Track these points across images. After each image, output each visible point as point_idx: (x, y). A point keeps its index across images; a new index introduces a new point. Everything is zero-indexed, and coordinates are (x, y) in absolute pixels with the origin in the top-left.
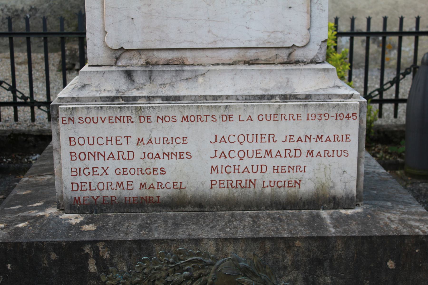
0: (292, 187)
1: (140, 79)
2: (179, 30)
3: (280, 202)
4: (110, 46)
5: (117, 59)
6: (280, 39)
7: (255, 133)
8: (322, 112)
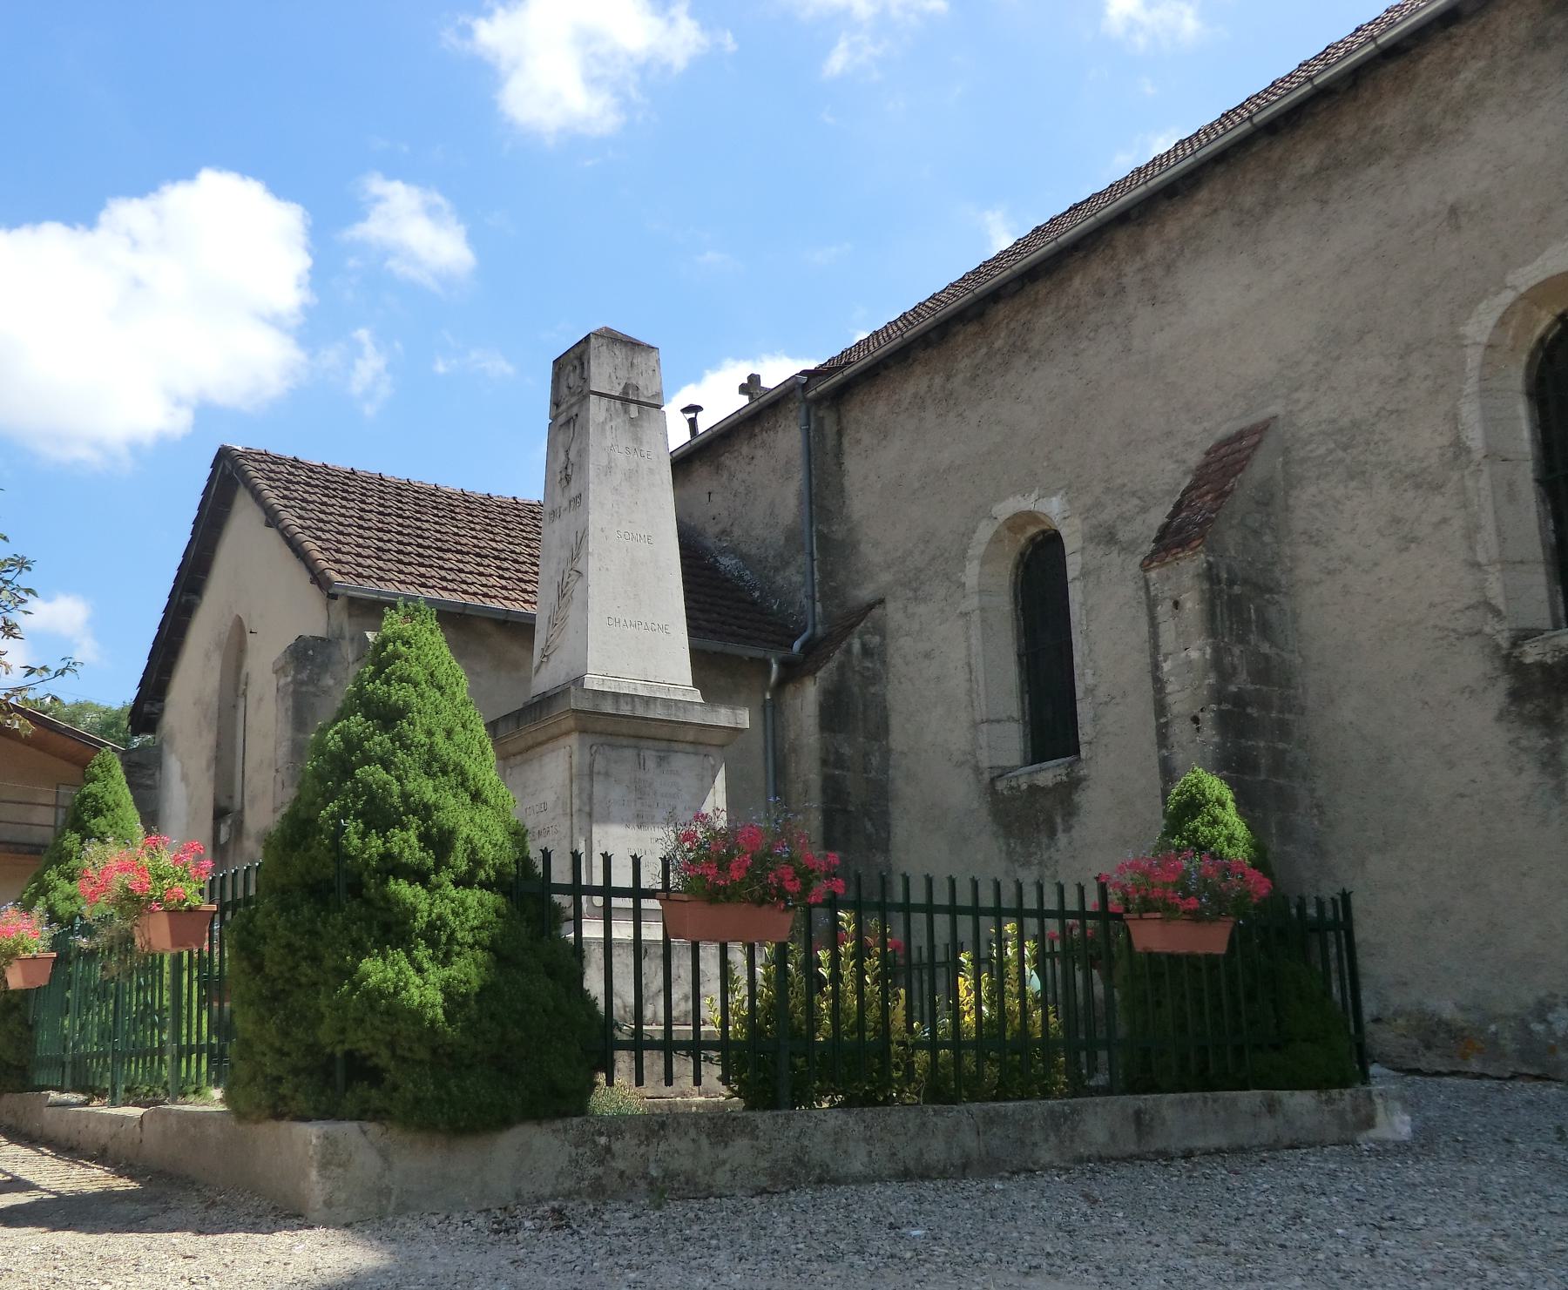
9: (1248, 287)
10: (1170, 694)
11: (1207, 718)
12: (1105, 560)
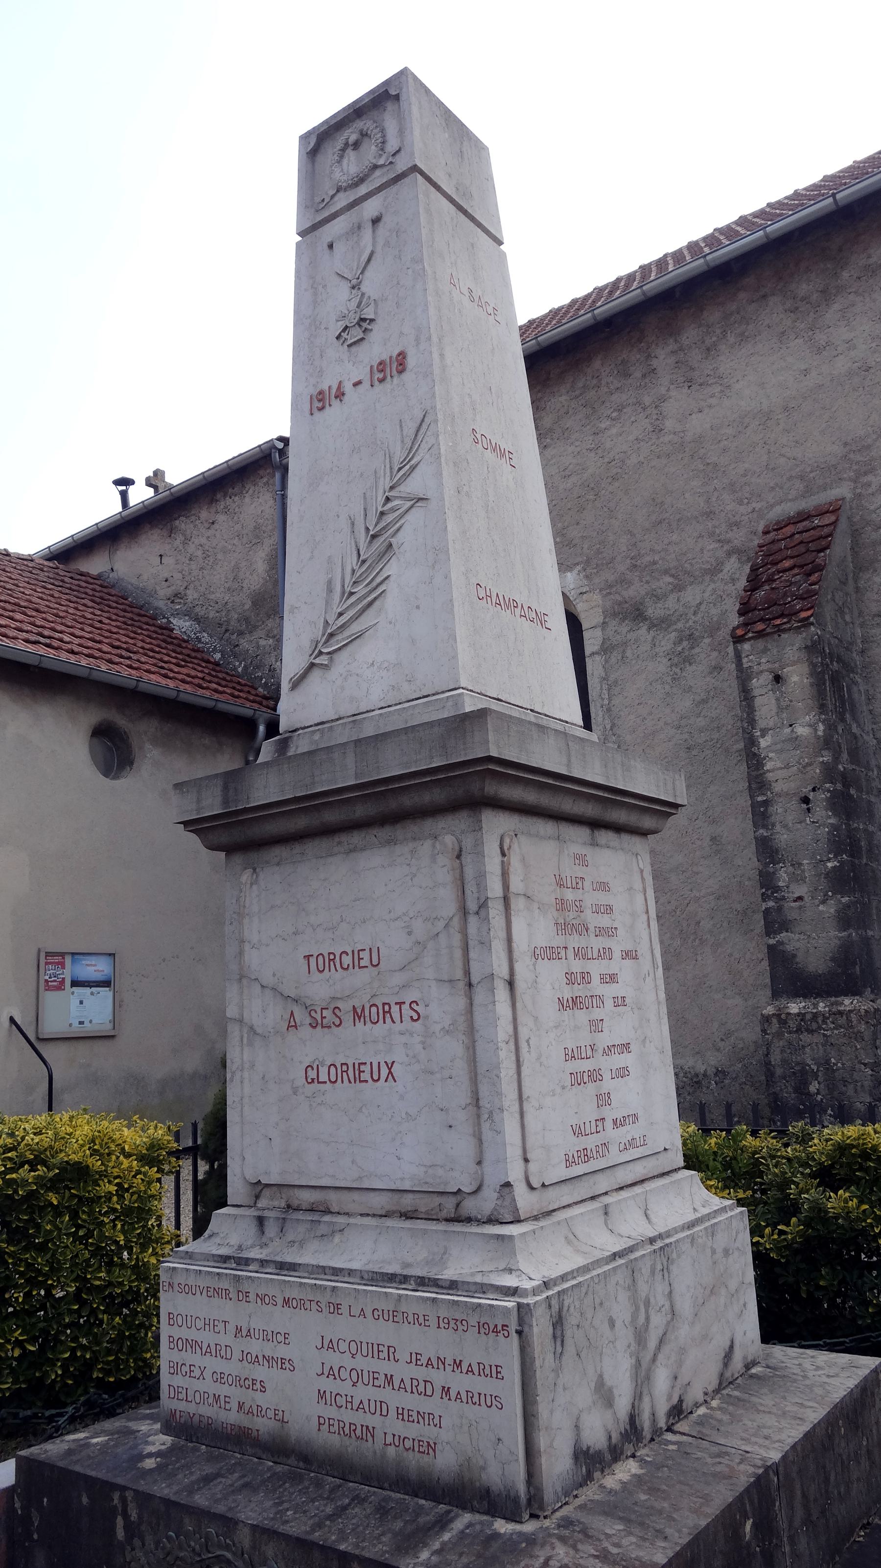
0: (424, 1453)
1: (271, 1229)
2: (319, 1158)
3: (409, 1480)
4: (247, 1178)
5: (257, 1197)
6: (440, 1177)
7: (370, 1342)
8: (458, 1316)
9: (805, 373)
10: (768, 771)
11: (820, 798)
12: (632, 636)
